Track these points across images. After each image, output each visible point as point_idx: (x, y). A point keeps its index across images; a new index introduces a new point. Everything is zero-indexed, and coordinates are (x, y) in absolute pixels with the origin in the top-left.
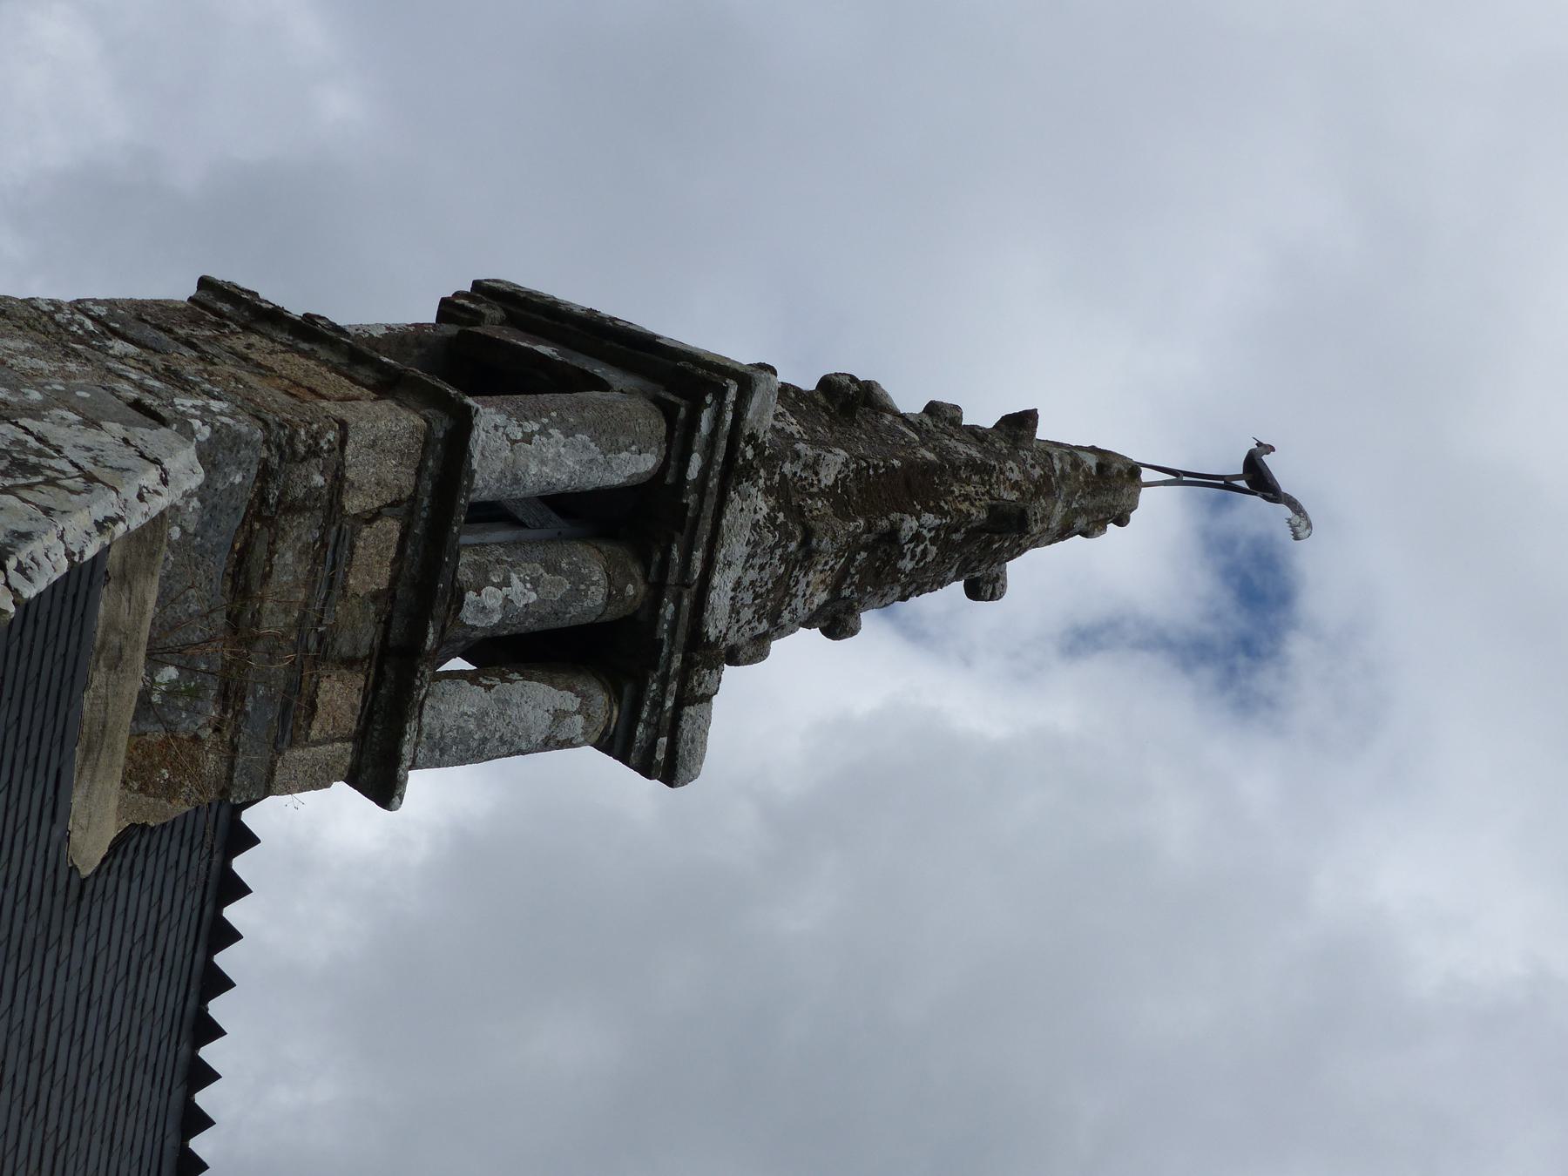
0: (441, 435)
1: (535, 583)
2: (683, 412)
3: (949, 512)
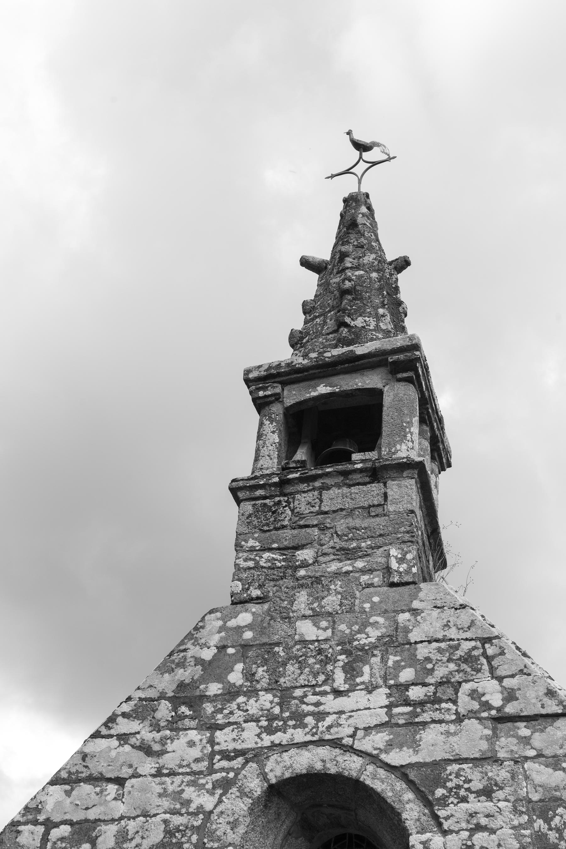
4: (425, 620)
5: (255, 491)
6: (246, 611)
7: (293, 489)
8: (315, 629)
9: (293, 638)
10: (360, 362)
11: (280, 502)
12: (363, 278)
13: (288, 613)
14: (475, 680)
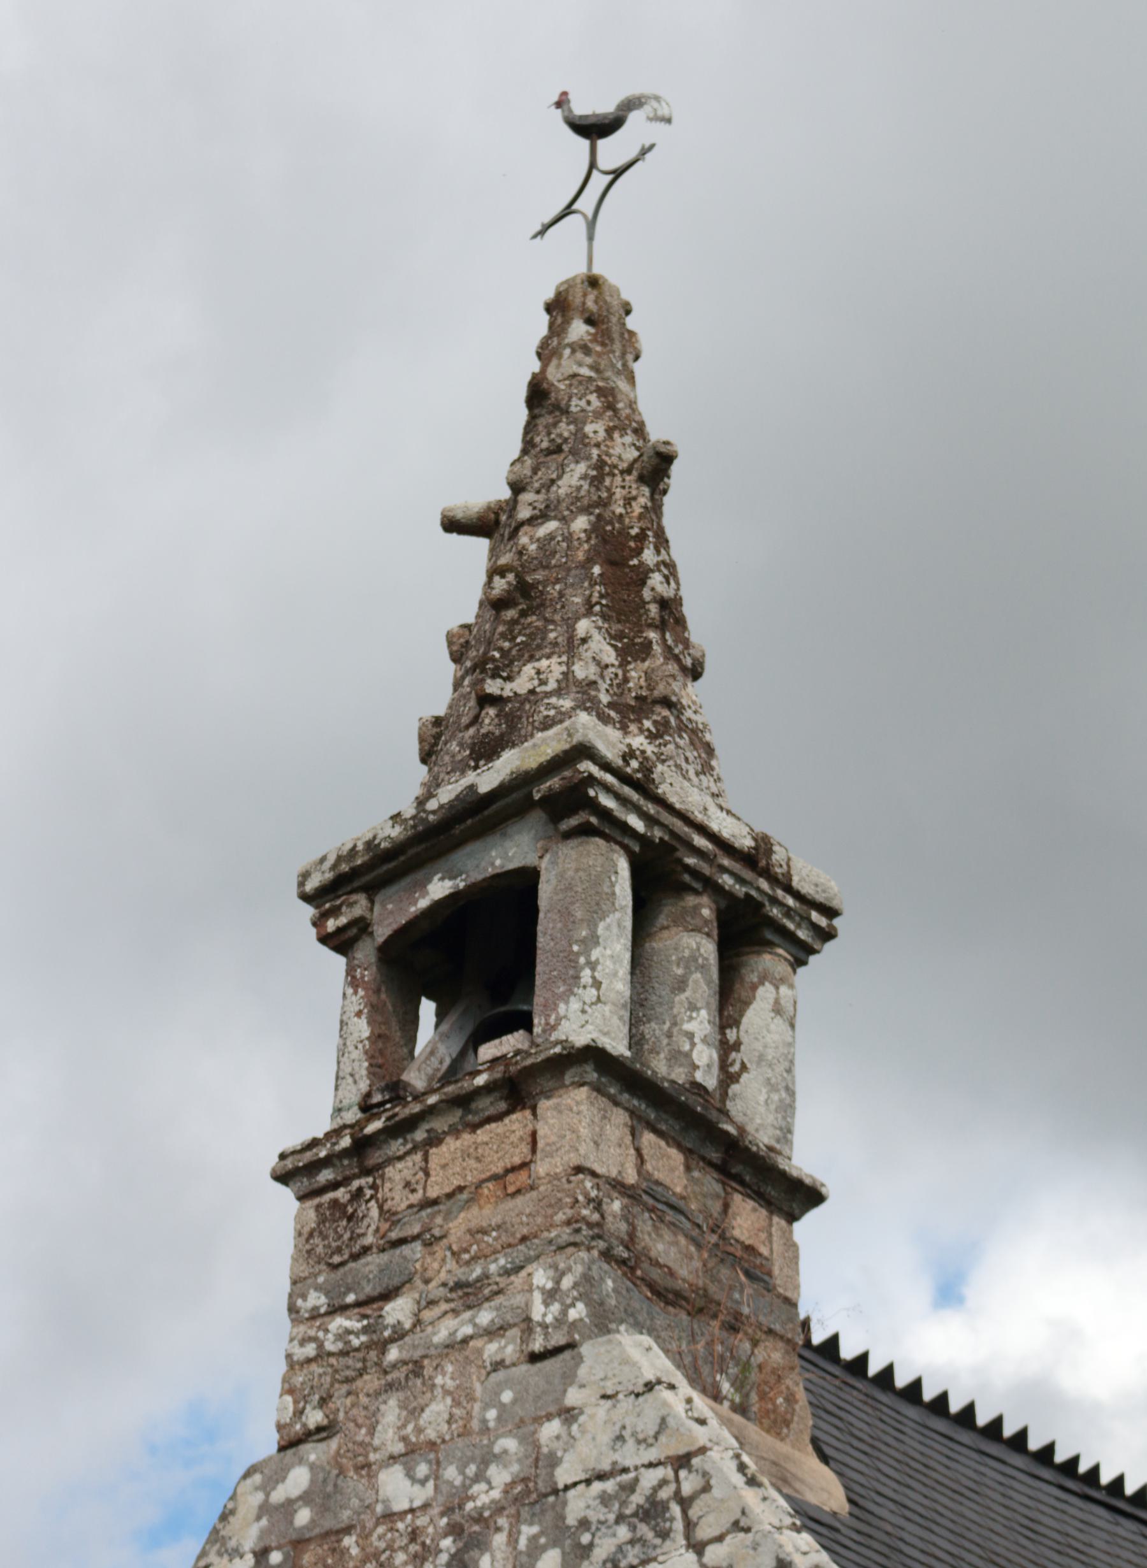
0: (595, 1075)
1: (693, 1007)
2: (593, 820)
3: (643, 530)
4: (583, 1432)
5: (317, 1174)
6: (301, 1461)
7: (380, 1156)
8: (408, 1483)
9: (373, 1512)
10: (494, 807)
11: (359, 1193)
12: (553, 543)
13: (366, 1456)
14: (660, 1558)
